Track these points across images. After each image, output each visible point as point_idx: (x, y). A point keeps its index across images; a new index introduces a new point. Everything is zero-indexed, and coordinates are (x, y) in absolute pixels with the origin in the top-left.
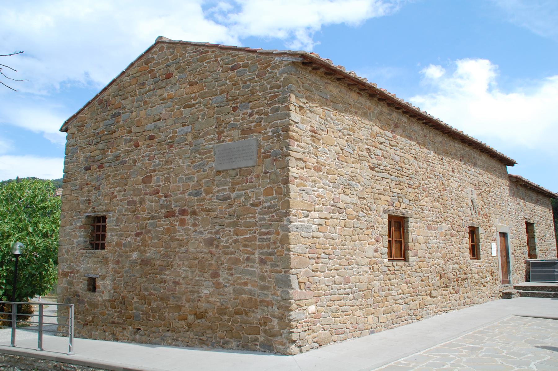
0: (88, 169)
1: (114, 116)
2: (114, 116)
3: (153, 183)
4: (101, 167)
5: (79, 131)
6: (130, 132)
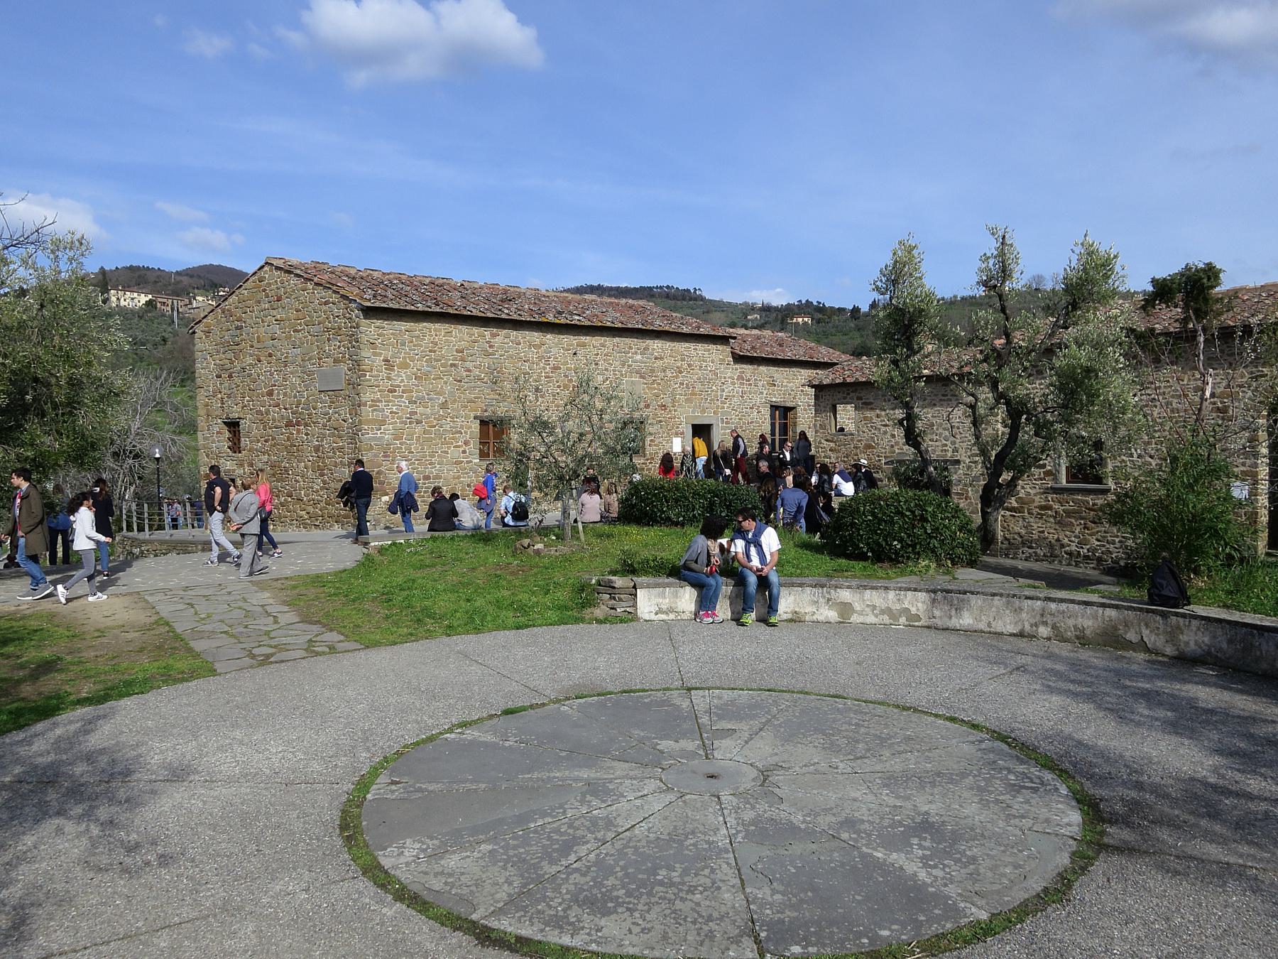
0: (219, 376)
1: (237, 328)
2: (237, 328)
3: (275, 397)
4: (230, 376)
5: (207, 337)
6: (252, 346)
